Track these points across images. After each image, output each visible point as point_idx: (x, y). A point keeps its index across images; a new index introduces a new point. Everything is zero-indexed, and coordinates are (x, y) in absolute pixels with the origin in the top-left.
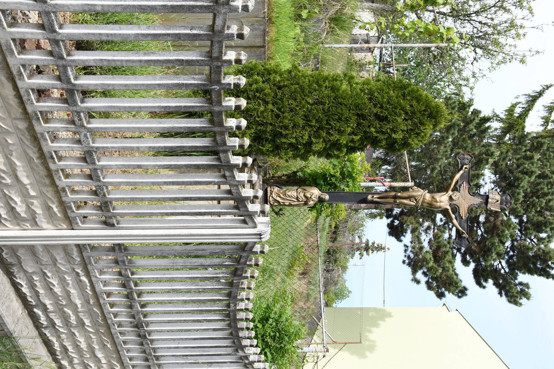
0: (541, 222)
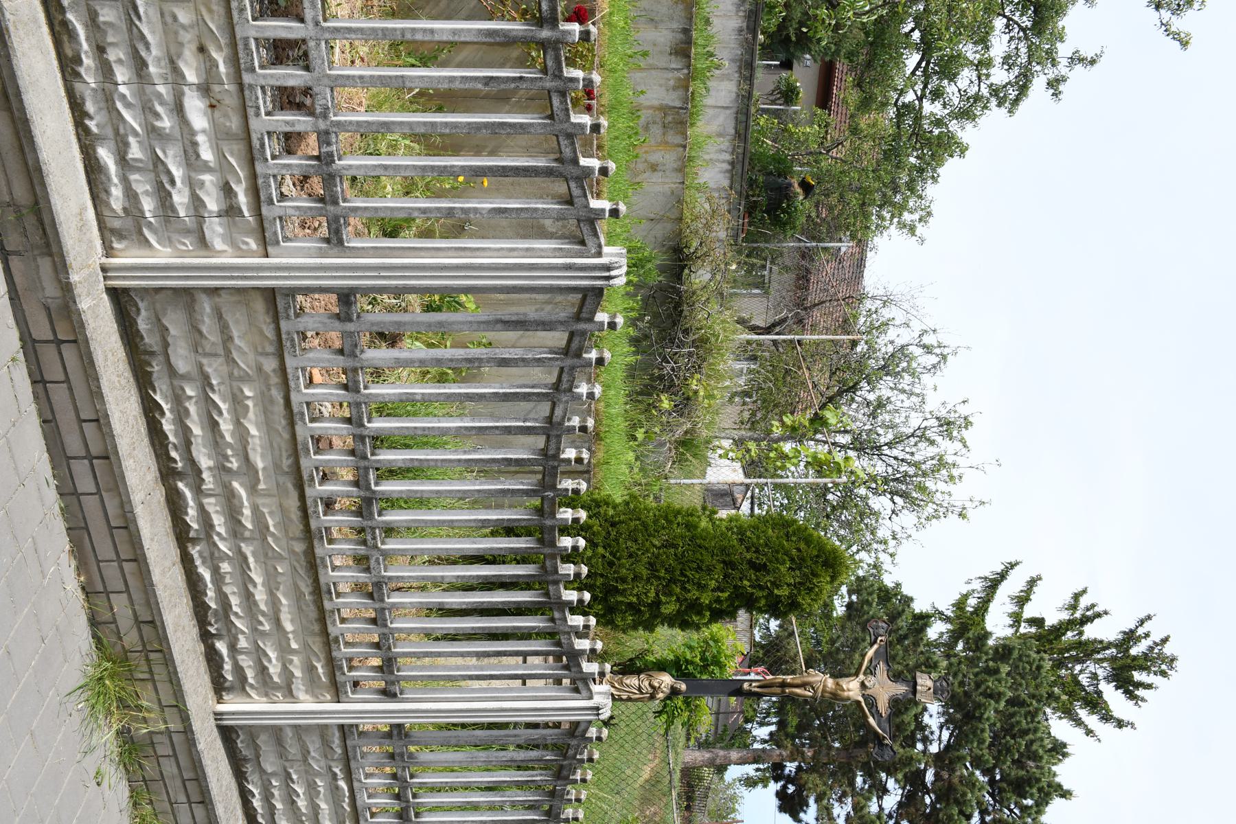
0: (1022, 778)
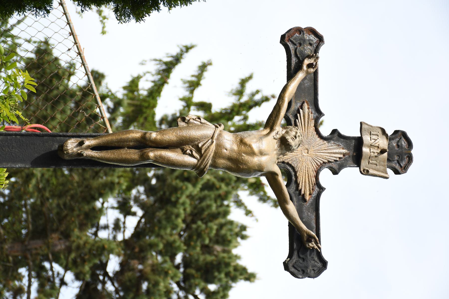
0: (211, 263)
